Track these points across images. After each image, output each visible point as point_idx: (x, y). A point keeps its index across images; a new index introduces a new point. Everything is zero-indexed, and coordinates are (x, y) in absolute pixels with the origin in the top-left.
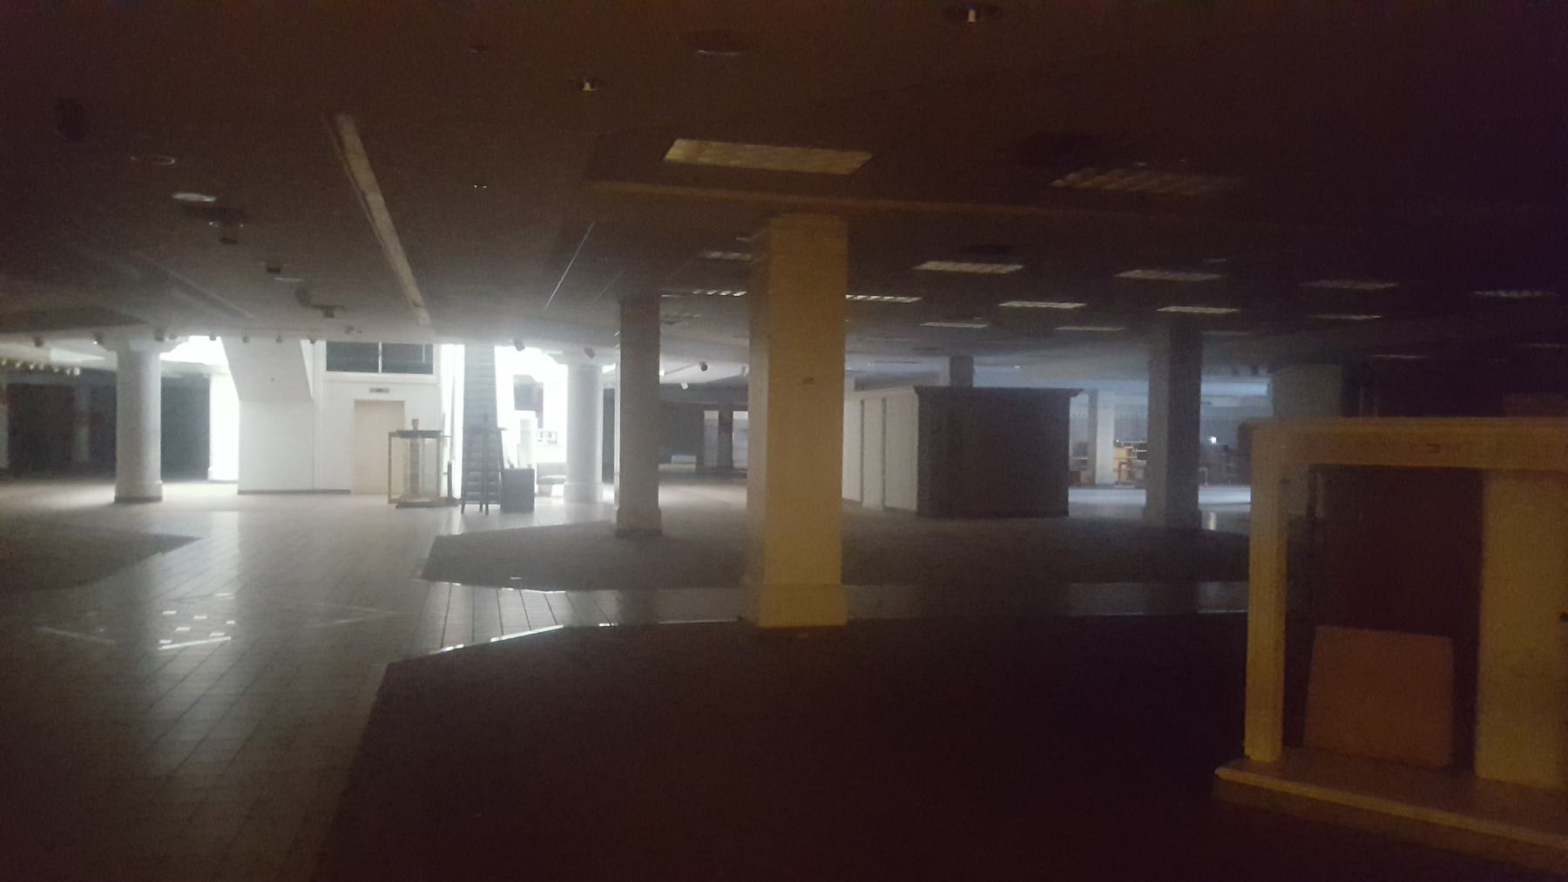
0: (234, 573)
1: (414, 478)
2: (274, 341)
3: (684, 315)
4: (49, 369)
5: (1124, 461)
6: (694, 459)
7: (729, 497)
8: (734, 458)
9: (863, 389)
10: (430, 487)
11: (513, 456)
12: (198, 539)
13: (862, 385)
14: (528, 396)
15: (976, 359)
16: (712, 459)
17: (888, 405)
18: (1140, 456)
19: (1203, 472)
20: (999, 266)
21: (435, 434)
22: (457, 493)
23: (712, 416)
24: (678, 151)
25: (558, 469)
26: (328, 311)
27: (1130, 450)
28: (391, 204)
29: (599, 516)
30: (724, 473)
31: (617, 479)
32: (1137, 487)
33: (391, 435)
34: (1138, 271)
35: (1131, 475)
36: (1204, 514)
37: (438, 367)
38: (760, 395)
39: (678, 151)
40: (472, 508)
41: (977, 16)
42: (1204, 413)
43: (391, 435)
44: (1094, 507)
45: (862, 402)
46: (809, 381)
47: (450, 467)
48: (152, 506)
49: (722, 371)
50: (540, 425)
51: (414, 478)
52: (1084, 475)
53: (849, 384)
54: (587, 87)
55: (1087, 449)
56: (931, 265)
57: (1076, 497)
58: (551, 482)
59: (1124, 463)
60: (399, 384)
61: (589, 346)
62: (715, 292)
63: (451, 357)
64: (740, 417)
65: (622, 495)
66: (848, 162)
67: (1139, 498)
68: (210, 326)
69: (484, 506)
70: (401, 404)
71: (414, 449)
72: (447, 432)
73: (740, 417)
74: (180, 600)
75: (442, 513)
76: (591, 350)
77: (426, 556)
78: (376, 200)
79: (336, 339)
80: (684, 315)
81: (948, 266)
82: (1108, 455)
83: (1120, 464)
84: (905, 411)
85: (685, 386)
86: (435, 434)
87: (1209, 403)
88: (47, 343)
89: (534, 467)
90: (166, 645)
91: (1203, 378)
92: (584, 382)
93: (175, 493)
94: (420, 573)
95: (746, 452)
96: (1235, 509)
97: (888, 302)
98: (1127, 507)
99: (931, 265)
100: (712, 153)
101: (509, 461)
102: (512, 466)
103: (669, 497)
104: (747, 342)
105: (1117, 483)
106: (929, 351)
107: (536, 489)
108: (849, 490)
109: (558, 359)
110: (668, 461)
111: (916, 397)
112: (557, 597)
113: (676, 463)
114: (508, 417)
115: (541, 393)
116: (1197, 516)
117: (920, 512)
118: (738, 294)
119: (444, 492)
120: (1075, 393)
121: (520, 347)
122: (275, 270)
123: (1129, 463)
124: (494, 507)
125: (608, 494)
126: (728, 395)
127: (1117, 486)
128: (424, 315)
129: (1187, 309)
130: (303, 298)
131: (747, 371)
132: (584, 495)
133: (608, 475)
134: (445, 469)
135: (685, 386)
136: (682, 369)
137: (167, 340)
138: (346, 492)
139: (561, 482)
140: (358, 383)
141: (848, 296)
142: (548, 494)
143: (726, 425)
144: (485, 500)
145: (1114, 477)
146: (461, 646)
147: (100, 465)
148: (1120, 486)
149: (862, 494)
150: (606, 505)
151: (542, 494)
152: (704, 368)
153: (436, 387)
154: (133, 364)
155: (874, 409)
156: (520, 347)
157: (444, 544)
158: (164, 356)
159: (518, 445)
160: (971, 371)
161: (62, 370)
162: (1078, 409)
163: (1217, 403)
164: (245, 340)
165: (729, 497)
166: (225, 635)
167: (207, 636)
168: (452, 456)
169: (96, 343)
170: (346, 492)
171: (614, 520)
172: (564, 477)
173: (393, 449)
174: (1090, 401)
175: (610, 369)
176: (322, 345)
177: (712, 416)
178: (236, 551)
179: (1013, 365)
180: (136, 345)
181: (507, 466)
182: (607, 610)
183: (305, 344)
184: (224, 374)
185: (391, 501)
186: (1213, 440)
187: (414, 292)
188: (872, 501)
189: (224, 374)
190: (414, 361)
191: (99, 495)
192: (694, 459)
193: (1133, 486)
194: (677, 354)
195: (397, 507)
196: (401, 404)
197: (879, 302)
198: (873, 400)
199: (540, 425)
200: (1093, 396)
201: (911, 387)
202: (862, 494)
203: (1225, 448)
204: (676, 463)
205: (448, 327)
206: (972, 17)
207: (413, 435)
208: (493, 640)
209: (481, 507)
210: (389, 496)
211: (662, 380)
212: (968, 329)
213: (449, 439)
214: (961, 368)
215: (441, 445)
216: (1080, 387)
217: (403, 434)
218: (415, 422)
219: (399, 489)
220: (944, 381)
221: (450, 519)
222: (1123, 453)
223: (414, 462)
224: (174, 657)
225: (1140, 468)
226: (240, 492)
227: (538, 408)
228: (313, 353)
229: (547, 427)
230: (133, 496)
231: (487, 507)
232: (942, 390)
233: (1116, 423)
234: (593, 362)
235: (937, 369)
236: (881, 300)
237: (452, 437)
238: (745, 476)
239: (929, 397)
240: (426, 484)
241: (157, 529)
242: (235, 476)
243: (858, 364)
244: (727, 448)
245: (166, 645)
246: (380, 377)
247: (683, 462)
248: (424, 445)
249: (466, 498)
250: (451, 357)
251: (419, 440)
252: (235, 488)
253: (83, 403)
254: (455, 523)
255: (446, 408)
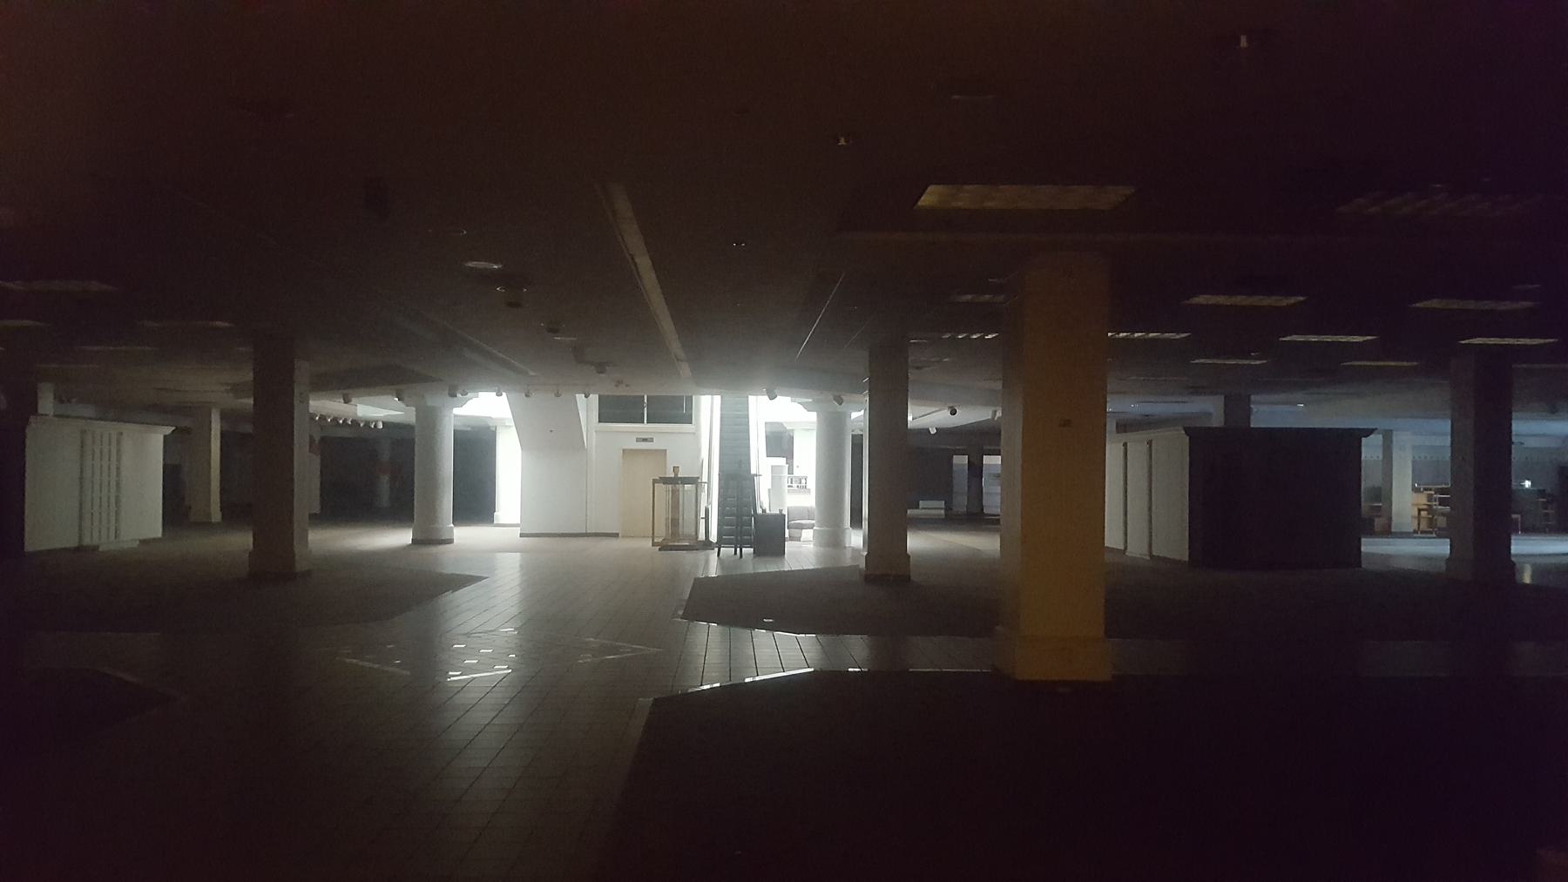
0: (514, 611)
1: (675, 523)
2: (553, 395)
3: (933, 360)
4: (355, 423)
5: (1425, 507)
6: (942, 504)
7: (985, 544)
8: (984, 504)
9: (1125, 431)
10: (690, 530)
11: (765, 501)
12: (479, 579)
13: (1124, 427)
14: (780, 444)
15: (1253, 398)
16: (961, 503)
17: (1154, 448)
18: (1442, 502)
19: (1517, 519)
20: (1244, 303)
21: (694, 481)
22: (714, 538)
23: (961, 461)
24: (931, 197)
25: (808, 514)
26: (601, 368)
27: (1432, 495)
28: (657, 266)
29: (848, 561)
30: (975, 519)
31: (865, 524)
32: (1439, 536)
33: (655, 481)
34: (1435, 301)
35: (1431, 522)
36: (1517, 566)
37: (698, 416)
38: (1013, 438)
39: (931, 197)
40: (728, 551)
41: (1249, 40)
42: (1516, 456)
43: (655, 481)
44: (1389, 557)
45: (1125, 445)
46: (1066, 423)
47: (707, 511)
48: (442, 548)
49: (970, 415)
50: (791, 471)
51: (675, 523)
52: (1379, 523)
53: (1111, 426)
54: (842, 142)
55: (1383, 494)
56: (1201, 299)
57: (1371, 546)
58: (802, 527)
59: (1423, 510)
60: (662, 434)
61: (837, 394)
62: (979, 335)
63: (708, 407)
64: (992, 461)
65: (871, 540)
66: (1113, 196)
67: (1442, 548)
68: (498, 386)
69: (738, 549)
70: (663, 453)
71: (675, 493)
72: (705, 479)
73: (992, 461)
74: (468, 635)
75: (701, 555)
76: (839, 397)
77: (687, 596)
78: (644, 263)
79: (602, 394)
80: (933, 360)
81: (1222, 300)
82: (1406, 502)
83: (1420, 510)
84: (1174, 450)
85: (933, 431)
86: (694, 481)
87: (1522, 444)
88: (354, 400)
89: (785, 512)
90: (455, 676)
91: (1514, 415)
92: (832, 431)
93: (465, 536)
94: (681, 613)
95: (999, 497)
96: (1553, 560)
97: (1153, 339)
98: (1429, 558)
99: (1201, 299)
100: (966, 197)
101: (761, 507)
102: (764, 511)
103: (917, 542)
104: (998, 385)
105: (1415, 532)
106: (1196, 390)
107: (787, 535)
108: (1113, 538)
109: (808, 408)
110: (917, 507)
111: (1187, 439)
112: (807, 639)
113: (923, 508)
114: (761, 464)
115: (791, 439)
116: (1508, 567)
117: (1194, 561)
118: (990, 337)
119: (702, 536)
120: (1368, 432)
121: (772, 397)
122: (554, 331)
123: (1430, 509)
124: (748, 551)
125: (856, 539)
126: (979, 440)
127: (1415, 535)
128: (685, 369)
129: (1344, 339)
130: (579, 356)
131: (999, 414)
132: (833, 539)
133: (856, 521)
134: (703, 514)
135: (933, 431)
136: (933, 412)
137: (459, 395)
138: (616, 535)
139: (811, 527)
140: (627, 433)
141: (1110, 334)
142: (798, 539)
143: (976, 469)
144: (739, 544)
145: (1411, 526)
146: (718, 685)
147: (400, 510)
148: (1419, 535)
149: (1126, 542)
150: (855, 550)
151: (792, 538)
152: (953, 412)
153: (696, 435)
154: (429, 420)
155: (1137, 449)
156: (772, 397)
157: (703, 586)
158: (456, 411)
159: (769, 490)
160: (1250, 410)
161: (367, 423)
162: (1370, 450)
163: (1532, 443)
164: (558, 395)
165: (985, 544)
166: (508, 668)
167: (492, 669)
168: (709, 502)
169: (397, 399)
170: (616, 535)
171: (863, 565)
172: (814, 522)
173: (652, 495)
174: (1384, 442)
175: (858, 416)
176: (594, 398)
177: (961, 461)
178: (518, 590)
179: (1295, 404)
180: (431, 401)
181: (759, 511)
182: (856, 654)
183: (580, 397)
184: (510, 426)
185: (654, 544)
186: (1527, 484)
187: (676, 346)
188: (1137, 549)
189: (510, 426)
190: (676, 412)
191: (400, 537)
192: (942, 504)
193: (1434, 535)
194: (926, 398)
195: (660, 550)
196: (663, 453)
197: (1145, 340)
198: (1137, 443)
199: (791, 471)
200: (1388, 436)
201: (1181, 428)
202: (1126, 542)
203: (1542, 493)
204: (923, 508)
205: (707, 377)
206: (1244, 42)
207: (675, 481)
208: (747, 680)
209: (736, 551)
210: (653, 540)
211: (910, 425)
212: (1384, 366)
213: (706, 485)
214: (1237, 406)
215: (699, 490)
216: (1374, 427)
217: (665, 481)
218: (675, 469)
219: (662, 531)
220: (1217, 421)
221: (707, 561)
222: (1422, 499)
223: (675, 505)
224: (463, 687)
225: (1443, 514)
226: (522, 535)
227: (789, 455)
228: (587, 406)
229: (797, 472)
230: (429, 538)
231: (741, 551)
232: (1210, 430)
233: (1414, 462)
234: (840, 408)
235: (1209, 409)
236: (1146, 337)
237: (709, 483)
238: (998, 522)
239: (1200, 439)
240: (687, 529)
241: (449, 570)
242: (518, 521)
243: (1120, 405)
244: (977, 493)
245: (455, 676)
246: (645, 427)
247: (932, 507)
248: (684, 491)
249: (719, 544)
250: (708, 407)
251: (680, 487)
252: (518, 531)
253: (385, 455)
254: (712, 565)
255: (704, 455)
